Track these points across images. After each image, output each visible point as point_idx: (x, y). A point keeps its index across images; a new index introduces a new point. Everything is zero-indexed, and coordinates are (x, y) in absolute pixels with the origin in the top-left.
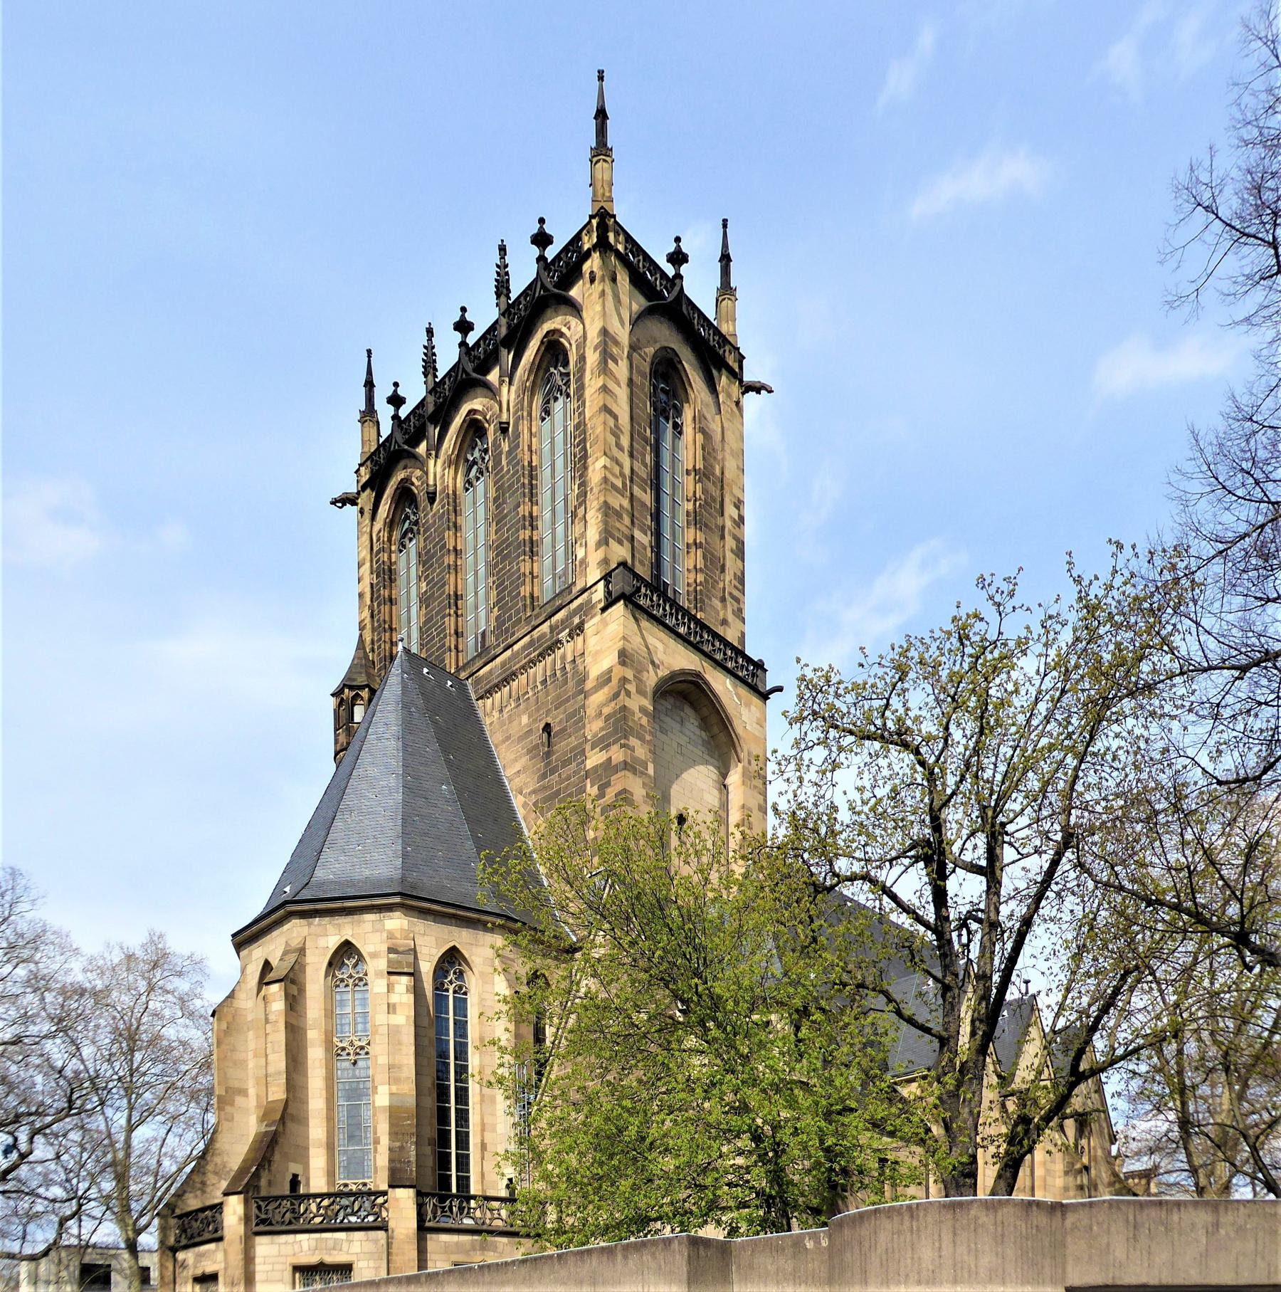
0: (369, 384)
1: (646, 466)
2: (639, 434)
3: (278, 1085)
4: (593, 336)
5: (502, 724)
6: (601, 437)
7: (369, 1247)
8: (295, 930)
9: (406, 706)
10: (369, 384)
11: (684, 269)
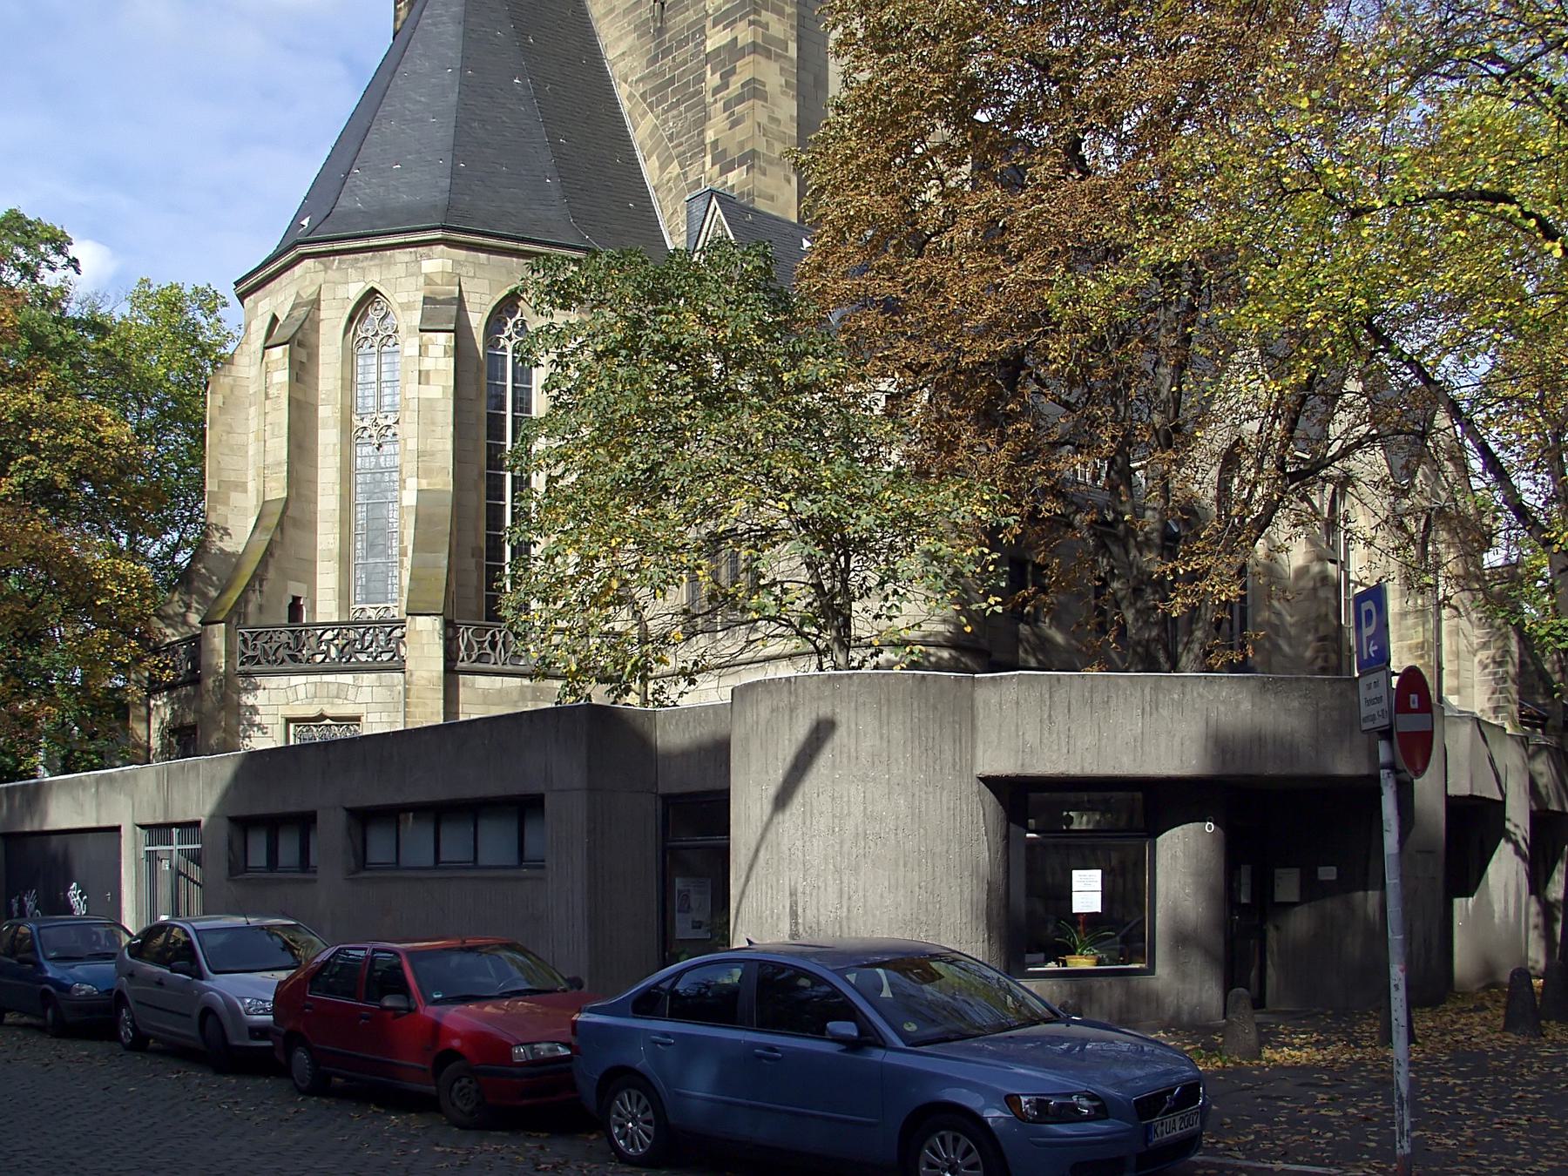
3: (276, 480)
7: (381, 694)
8: (305, 277)
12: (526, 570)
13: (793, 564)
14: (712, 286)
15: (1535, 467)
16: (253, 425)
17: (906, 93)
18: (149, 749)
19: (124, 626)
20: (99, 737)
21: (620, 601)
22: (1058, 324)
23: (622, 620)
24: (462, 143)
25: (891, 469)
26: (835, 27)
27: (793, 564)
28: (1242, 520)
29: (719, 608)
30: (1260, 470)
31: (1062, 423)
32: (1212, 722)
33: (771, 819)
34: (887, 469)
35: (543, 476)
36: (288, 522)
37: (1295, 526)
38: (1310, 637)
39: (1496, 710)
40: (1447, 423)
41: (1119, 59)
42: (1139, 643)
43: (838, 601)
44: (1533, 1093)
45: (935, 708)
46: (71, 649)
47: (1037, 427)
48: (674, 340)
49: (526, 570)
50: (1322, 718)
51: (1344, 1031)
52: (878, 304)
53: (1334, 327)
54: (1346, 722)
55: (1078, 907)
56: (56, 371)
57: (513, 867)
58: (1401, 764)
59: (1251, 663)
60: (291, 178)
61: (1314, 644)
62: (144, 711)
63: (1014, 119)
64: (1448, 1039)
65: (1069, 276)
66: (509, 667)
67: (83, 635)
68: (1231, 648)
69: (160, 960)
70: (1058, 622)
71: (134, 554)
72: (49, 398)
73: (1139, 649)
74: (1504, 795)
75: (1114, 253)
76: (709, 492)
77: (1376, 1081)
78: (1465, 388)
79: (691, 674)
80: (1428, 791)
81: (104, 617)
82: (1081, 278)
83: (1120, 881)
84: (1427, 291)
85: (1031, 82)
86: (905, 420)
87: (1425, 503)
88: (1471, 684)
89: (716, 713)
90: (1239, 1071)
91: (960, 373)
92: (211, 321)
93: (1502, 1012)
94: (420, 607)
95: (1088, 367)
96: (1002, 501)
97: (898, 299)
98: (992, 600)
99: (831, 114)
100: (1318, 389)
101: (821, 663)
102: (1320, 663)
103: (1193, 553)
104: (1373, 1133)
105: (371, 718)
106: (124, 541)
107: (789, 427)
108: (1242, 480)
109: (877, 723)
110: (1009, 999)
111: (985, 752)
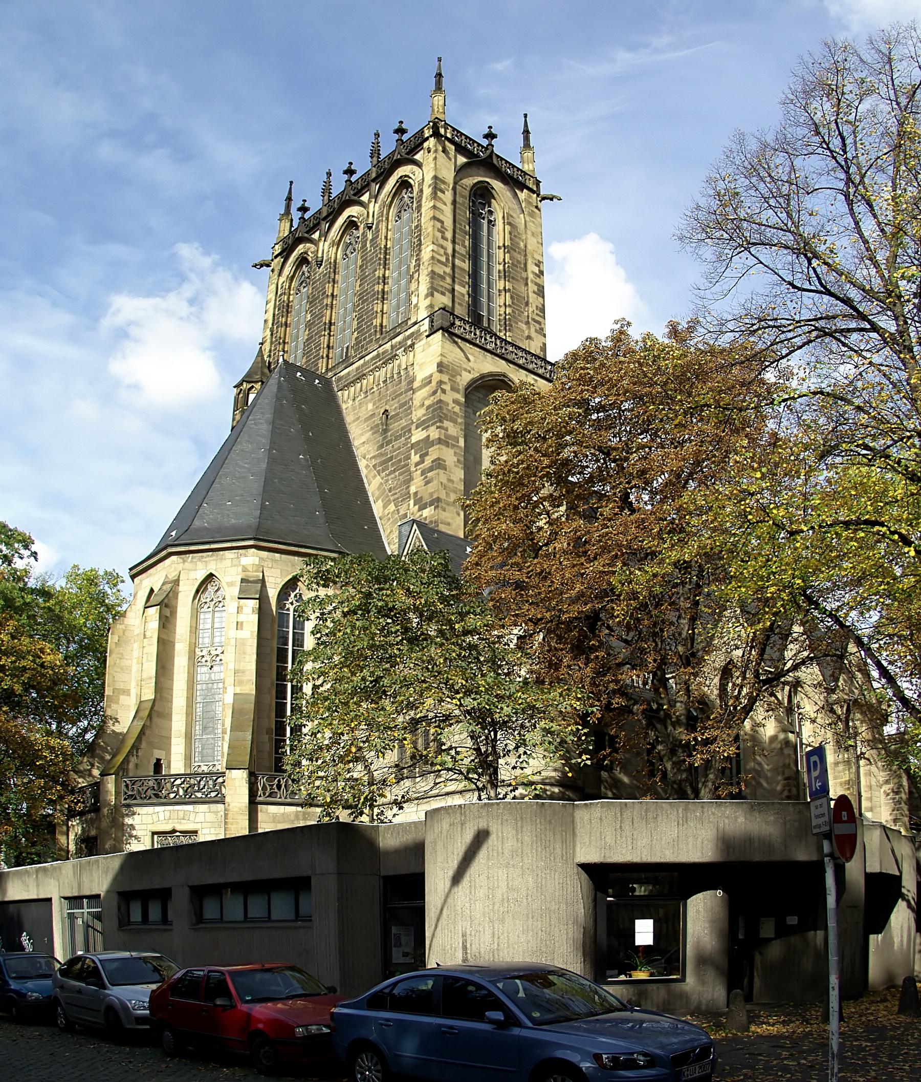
0: (289, 199)
1: (465, 247)
2: (460, 229)
4: (428, 180)
5: (354, 409)
6: (431, 234)
7: (210, 817)
9: (278, 399)
10: (289, 199)
11: (494, 142)
12: (299, 741)
13: (462, 737)
14: (413, 574)
15: (911, 675)
16: (136, 654)
17: (528, 468)
18: (68, 851)
19: (53, 777)
20: (35, 844)
21: (356, 760)
22: (619, 595)
23: (358, 771)
24: (268, 489)
25: (521, 679)
26: (486, 431)
27: (462, 737)
28: (735, 708)
29: (418, 763)
30: (744, 678)
31: (624, 652)
32: (721, 830)
33: (450, 891)
34: (518, 679)
35: (310, 685)
36: (154, 713)
37: (768, 711)
38: (780, 778)
39: (895, 821)
40: (855, 650)
41: (650, 448)
42: (674, 782)
43: (490, 758)
44: (913, 1050)
45: (550, 822)
46: (20, 791)
47: (609, 654)
48: (390, 605)
49: (299, 741)
50: (788, 826)
51: (800, 1015)
52: (512, 584)
53: (784, 595)
54: (802, 829)
55: (638, 942)
56: (18, 621)
57: (292, 921)
58: (837, 854)
59: (744, 794)
60: (164, 509)
61: (782, 782)
62: (65, 828)
63: (591, 480)
64: (864, 1019)
65: (625, 568)
66: (289, 800)
67: (28, 783)
68: (731, 784)
69: (78, 978)
70: (624, 769)
71: (60, 734)
72: (13, 637)
73: (675, 786)
74: (901, 873)
75: (652, 555)
76: (411, 694)
77: (818, 1044)
78: (864, 628)
79: (401, 803)
80: (854, 870)
81: (41, 772)
82: (632, 569)
83: (664, 926)
84: (838, 575)
85: (599, 461)
86: (529, 651)
87: (846, 697)
88: (879, 805)
89: (416, 827)
90: (735, 1039)
91: (562, 623)
92: (114, 591)
93: (897, 1003)
94: (234, 764)
95: (638, 620)
96: (589, 698)
97: (524, 582)
98: (584, 757)
99: (483, 478)
100: (777, 631)
101: (480, 796)
102: (786, 793)
103: (706, 728)
104: (815, 1075)
105: (205, 831)
106: (54, 727)
107: (459, 655)
108: (734, 684)
109: (514, 832)
110: (597, 997)
111: (581, 848)
